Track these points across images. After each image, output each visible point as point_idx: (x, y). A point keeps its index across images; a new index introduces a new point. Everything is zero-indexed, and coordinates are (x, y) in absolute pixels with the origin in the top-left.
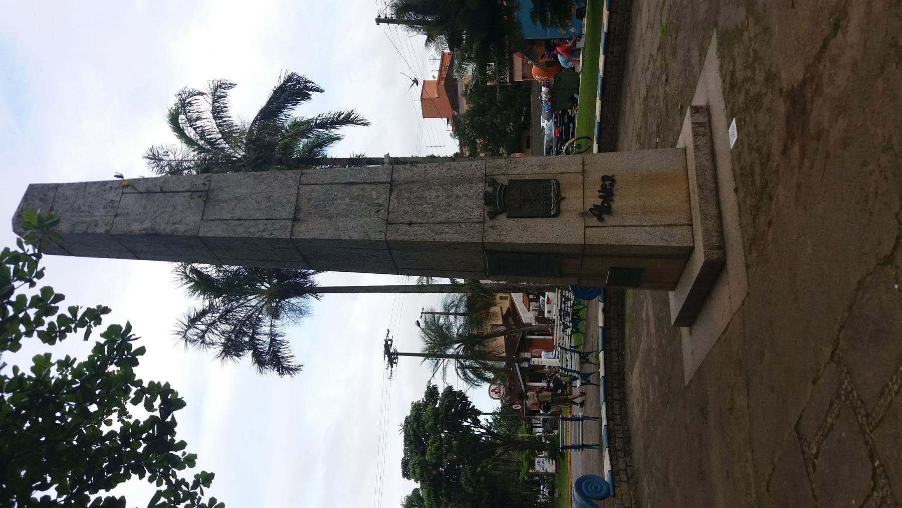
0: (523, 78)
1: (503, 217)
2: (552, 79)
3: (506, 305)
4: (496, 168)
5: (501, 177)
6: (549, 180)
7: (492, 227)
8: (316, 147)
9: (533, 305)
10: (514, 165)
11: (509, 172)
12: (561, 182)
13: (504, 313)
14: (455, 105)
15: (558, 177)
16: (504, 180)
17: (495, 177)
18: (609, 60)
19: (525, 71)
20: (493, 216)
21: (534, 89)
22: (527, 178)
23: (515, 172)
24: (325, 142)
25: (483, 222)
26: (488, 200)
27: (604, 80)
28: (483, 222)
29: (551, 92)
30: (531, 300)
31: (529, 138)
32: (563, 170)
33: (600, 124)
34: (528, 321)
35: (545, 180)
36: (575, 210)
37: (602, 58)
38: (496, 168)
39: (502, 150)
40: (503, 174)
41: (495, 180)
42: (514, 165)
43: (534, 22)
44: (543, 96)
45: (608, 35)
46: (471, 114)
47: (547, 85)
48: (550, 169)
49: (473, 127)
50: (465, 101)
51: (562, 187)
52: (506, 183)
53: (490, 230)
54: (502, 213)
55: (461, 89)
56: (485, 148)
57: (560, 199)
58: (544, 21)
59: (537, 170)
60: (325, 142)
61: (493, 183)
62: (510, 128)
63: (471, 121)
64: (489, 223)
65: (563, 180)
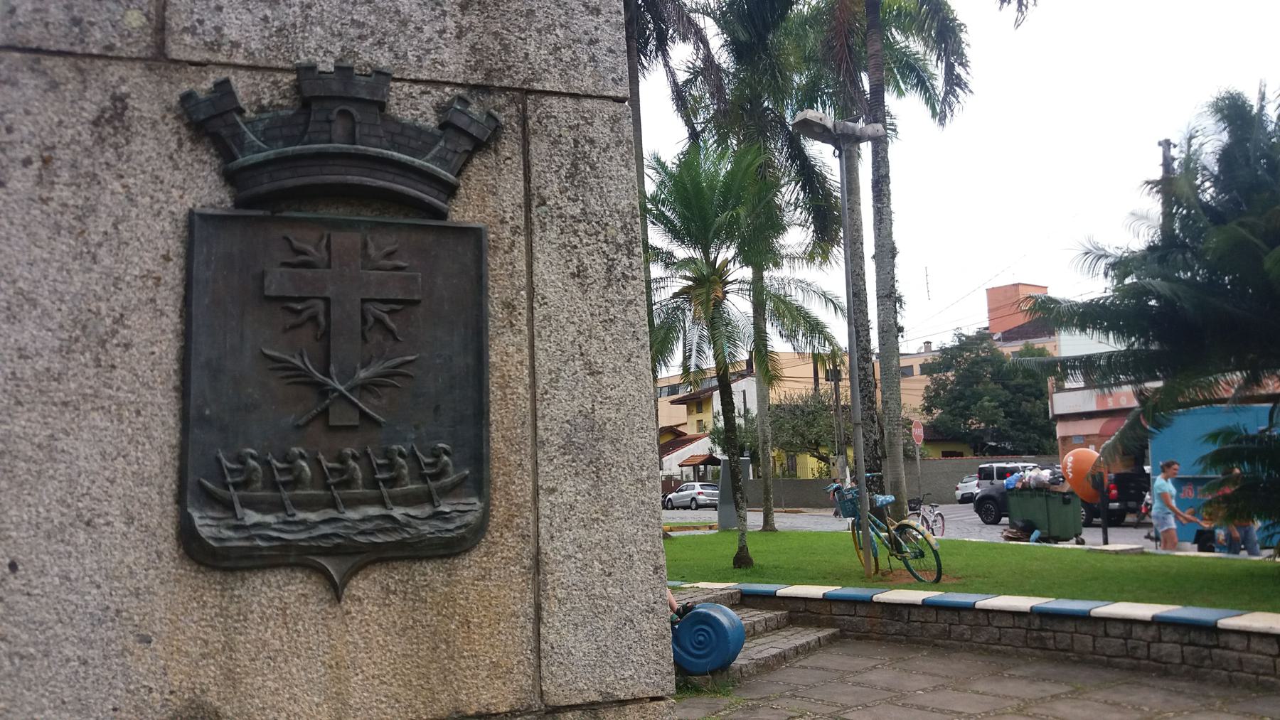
0: (1064, 439)
1: (203, 188)
2: (1066, 487)
3: (691, 431)
4: (578, 158)
5: (512, 190)
6: (479, 483)
7: (115, 115)
8: (919, 76)
9: (688, 471)
10: (596, 267)
11: (548, 241)
12: (468, 566)
13: (680, 429)
14: (1009, 336)
15: (504, 546)
16: (486, 198)
17: (509, 146)
18: (1138, 631)
19: (1075, 441)
20: (209, 121)
21: (1045, 459)
22: (505, 350)
23: (549, 272)
24: (927, 90)
25: (158, 58)
26: (334, 98)
27: (1085, 618)
28: (158, 58)
29: (1040, 489)
30: (695, 467)
31: (961, 455)
32: (561, 574)
33: (971, 608)
34: (665, 465)
35: (478, 458)
36: (231, 677)
37: (1144, 611)
38: (578, 158)
39: (937, 412)
40: (529, 199)
41: (481, 145)
42: (596, 267)
43: (1214, 437)
44: (1034, 473)
45: (1211, 629)
46: (996, 359)
47: (1055, 481)
48: (568, 488)
49: (975, 363)
50: (1017, 349)
51: (431, 572)
52: (462, 213)
53: (94, 102)
54: (230, 177)
55: (1038, 343)
56: (941, 385)
57: (335, 564)
58: (1217, 459)
59: (560, 409)
60: (927, 90)
61: (469, 135)
62: (975, 424)
63: (984, 360)
64: (151, 99)
65: (486, 580)
